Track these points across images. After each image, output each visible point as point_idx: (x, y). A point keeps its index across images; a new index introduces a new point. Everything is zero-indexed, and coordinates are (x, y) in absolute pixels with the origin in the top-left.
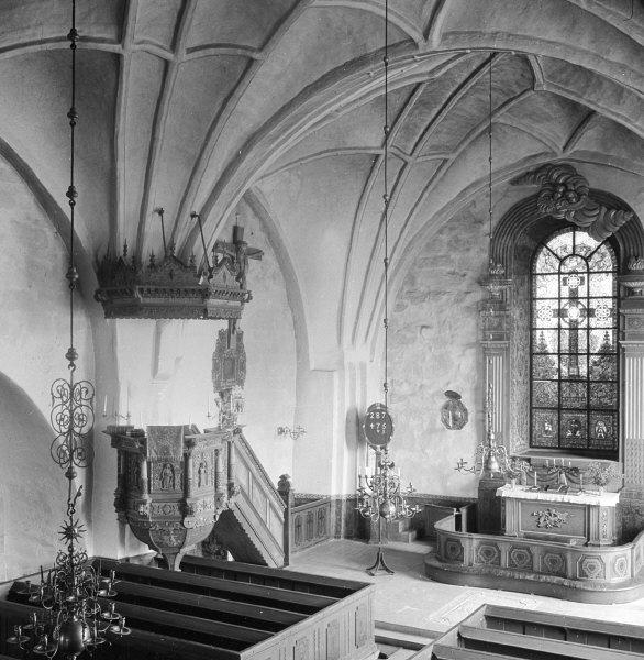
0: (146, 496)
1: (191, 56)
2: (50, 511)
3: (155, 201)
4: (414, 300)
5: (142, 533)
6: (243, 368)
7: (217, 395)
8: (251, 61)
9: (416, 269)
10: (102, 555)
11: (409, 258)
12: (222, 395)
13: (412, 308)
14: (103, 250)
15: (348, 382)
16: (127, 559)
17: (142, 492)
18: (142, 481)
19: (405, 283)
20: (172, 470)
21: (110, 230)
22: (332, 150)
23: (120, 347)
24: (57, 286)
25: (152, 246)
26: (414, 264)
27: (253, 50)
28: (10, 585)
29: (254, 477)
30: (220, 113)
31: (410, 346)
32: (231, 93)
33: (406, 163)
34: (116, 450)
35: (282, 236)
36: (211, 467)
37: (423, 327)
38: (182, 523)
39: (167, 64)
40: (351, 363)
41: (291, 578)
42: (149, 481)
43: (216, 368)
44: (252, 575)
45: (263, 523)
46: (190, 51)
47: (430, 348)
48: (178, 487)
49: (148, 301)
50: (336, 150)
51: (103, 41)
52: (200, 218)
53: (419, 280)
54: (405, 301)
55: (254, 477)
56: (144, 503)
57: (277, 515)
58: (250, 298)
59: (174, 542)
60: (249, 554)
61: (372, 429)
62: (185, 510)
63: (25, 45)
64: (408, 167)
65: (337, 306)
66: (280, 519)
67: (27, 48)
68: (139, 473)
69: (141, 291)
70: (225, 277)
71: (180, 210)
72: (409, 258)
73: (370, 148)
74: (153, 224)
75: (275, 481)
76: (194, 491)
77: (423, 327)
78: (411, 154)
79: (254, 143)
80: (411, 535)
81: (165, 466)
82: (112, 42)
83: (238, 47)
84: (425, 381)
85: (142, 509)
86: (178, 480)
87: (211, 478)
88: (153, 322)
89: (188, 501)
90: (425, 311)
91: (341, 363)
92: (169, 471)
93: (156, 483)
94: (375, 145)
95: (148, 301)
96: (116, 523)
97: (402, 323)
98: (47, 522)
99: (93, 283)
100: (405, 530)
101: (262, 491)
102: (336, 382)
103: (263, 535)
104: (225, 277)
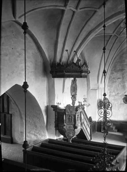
0: (65, 124)
1: (81, 10)
2: (37, 127)
3: (66, 48)
4: (116, 72)
5: (62, 132)
6: (77, 89)
7: (71, 96)
8: (95, 12)
9: (116, 64)
10: (51, 138)
11: (115, 61)
12: (73, 96)
13: (115, 74)
14: (52, 61)
15: (100, 93)
16: (57, 139)
17: (64, 123)
18: (64, 120)
19: (113, 67)
20: (71, 117)
21: (54, 56)
22: (100, 34)
23: (55, 85)
24: (41, 69)
25: (64, 60)
26: (116, 62)
27: (97, 9)
28: (32, 147)
29: (85, 118)
30: (85, 25)
31: (115, 83)
32: (89, 20)
33: (118, 37)
34: (54, 112)
35: (85, 56)
36: (80, 116)
37: (118, 78)
38: (74, 131)
39: (74, 12)
40: (101, 88)
41: (111, 146)
42: (66, 120)
43: (71, 90)
44: (83, 142)
45: (86, 129)
46: (80, 9)
47: (120, 84)
48: (73, 121)
49: (66, 74)
50: (101, 34)
51: (61, 6)
52: (76, 52)
53: (117, 66)
54: (113, 72)
55: (85, 118)
56: (65, 125)
57: (89, 127)
58: (90, 72)
59: (71, 135)
60: (85, 138)
61: (104, 105)
62: (75, 127)
63: (41, 8)
64: (118, 38)
65: (97, 73)
66: (89, 128)
67: (85, 9)
68: (63, 118)
69: (65, 71)
70: (85, 67)
71: (72, 50)
72: (115, 61)
73: (110, 34)
74: (65, 54)
75: (88, 118)
76: (77, 123)
77: (118, 78)
78: (119, 35)
79: (91, 34)
80: (116, 130)
81: (69, 116)
82: (63, 7)
83: (93, 8)
84: (119, 92)
85: (64, 127)
86: (73, 120)
87: (80, 119)
88: (63, 79)
89: (76, 125)
90: (119, 75)
91: (98, 88)
92: (70, 117)
93: (67, 120)
94: (111, 33)
95: (66, 74)
96: (54, 130)
97: (113, 77)
98: (36, 130)
99: (50, 69)
100: (115, 129)
101: (86, 121)
102: (97, 92)
103: (86, 131)
104: (85, 67)
